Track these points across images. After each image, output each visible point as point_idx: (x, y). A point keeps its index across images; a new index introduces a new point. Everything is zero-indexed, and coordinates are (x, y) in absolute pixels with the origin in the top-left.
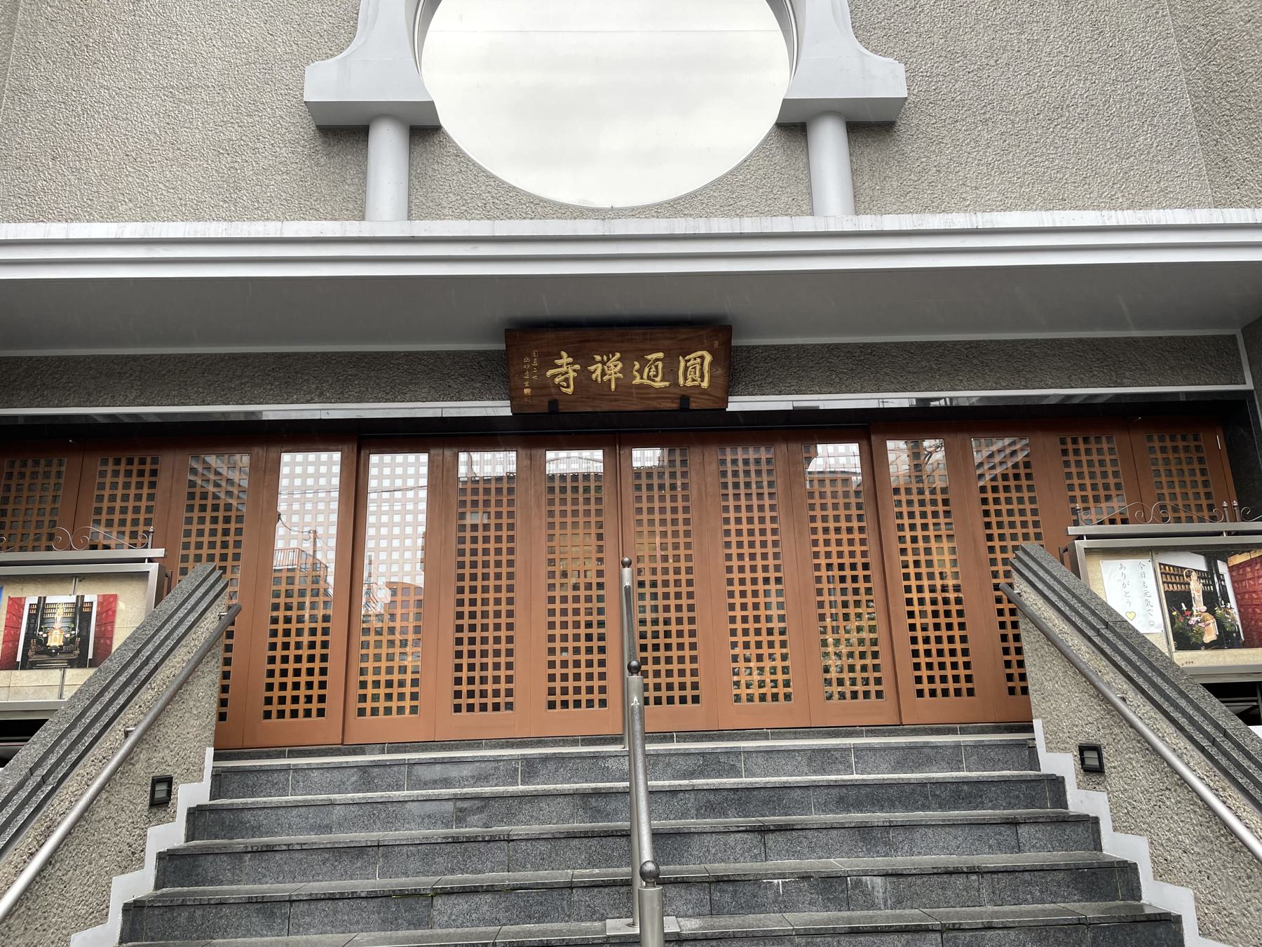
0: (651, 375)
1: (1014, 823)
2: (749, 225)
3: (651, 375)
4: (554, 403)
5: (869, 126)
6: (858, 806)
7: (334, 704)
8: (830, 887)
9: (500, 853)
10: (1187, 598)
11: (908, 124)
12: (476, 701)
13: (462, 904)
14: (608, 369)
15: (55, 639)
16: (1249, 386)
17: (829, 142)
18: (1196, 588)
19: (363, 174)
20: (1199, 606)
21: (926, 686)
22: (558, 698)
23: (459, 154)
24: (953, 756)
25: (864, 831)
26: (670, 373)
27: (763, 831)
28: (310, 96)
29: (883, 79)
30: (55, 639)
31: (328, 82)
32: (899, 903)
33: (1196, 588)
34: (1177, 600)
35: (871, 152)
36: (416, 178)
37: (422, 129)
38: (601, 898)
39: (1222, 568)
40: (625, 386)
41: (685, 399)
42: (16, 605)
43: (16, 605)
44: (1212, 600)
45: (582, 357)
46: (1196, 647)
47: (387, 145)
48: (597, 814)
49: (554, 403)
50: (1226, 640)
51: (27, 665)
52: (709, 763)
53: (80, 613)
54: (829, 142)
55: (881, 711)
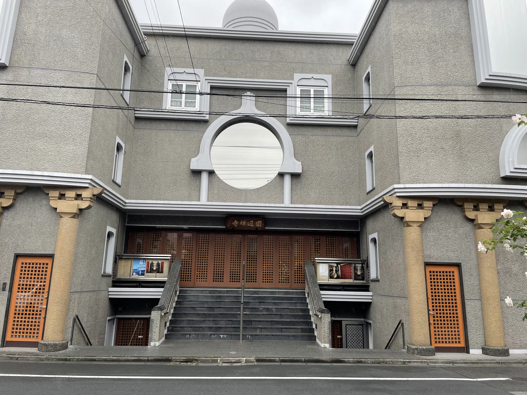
0: (251, 224)
1: (296, 303)
2: (267, 205)
3: (251, 224)
4: (233, 228)
5: (295, 176)
6: (276, 300)
7: (192, 279)
8: (268, 310)
9: (223, 303)
10: (333, 270)
11: (302, 177)
12: (269, 281)
13: (218, 309)
14: (243, 223)
15: (155, 268)
16: (359, 230)
17: (287, 179)
18: (334, 269)
19: (200, 181)
20: (334, 272)
21: (296, 281)
22: (280, 281)
23: (218, 177)
24: (292, 293)
25: (275, 303)
26: (254, 224)
27: (260, 302)
28: (192, 167)
29: (298, 169)
30: (155, 268)
31: (195, 165)
32: (277, 312)
33: (334, 269)
34: (331, 271)
35: (295, 181)
36: (210, 182)
37: (211, 173)
38: (237, 309)
39: (339, 266)
40: (246, 226)
41: (257, 228)
42: (148, 263)
43: (148, 263)
44: (336, 271)
45: (239, 221)
46: (333, 278)
47: (205, 177)
48: (237, 299)
49: (233, 228)
50: (338, 277)
51: (150, 272)
52: (255, 293)
53: (158, 264)
54: (287, 179)
55: (288, 285)
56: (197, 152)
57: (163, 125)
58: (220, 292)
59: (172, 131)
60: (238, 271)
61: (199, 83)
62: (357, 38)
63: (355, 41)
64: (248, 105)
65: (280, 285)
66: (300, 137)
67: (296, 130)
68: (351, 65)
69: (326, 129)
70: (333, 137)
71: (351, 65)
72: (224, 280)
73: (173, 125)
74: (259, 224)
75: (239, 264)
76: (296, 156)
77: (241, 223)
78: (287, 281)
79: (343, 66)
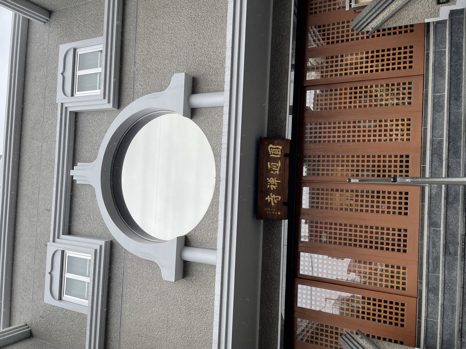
0: (276, 167)
3: (276, 167)
4: (284, 204)
5: (194, 86)
7: (401, 300)
14: (273, 183)
17: (199, 100)
21: (408, 65)
23: (195, 230)
24: (439, 54)
26: (276, 160)
29: (178, 81)
31: (169, 272)
35: (202, 85)
36: (201, 246)
37: (186, 242)
40: (279, 177)
41: (286, 155)
45: (268, 192)
47: (191, 255)
48: (456, 198)
49: (284, 204)
52: (436, 152)
55: (417, 84)
56: (153, 266)
57: (114, 320)
58: (433, 244)
59: (124, 306)
60: (398, 196)
61: (69, 253)
62: (18, 13)
63: (22, 15)
64: (89, 174)
65: (417, 100)
66: (137, 84)
67: (127, 91)
68: (50, 17)
69: (126, 42)
70: (138, 27)
71: (50, 17)
72: (403, 227)
73: (115, 301)
74: (275, 150)
75: (387, 195)
76: (162, 87)
77: (273, 187)
78: (407, 86)
79: (51, 29)
